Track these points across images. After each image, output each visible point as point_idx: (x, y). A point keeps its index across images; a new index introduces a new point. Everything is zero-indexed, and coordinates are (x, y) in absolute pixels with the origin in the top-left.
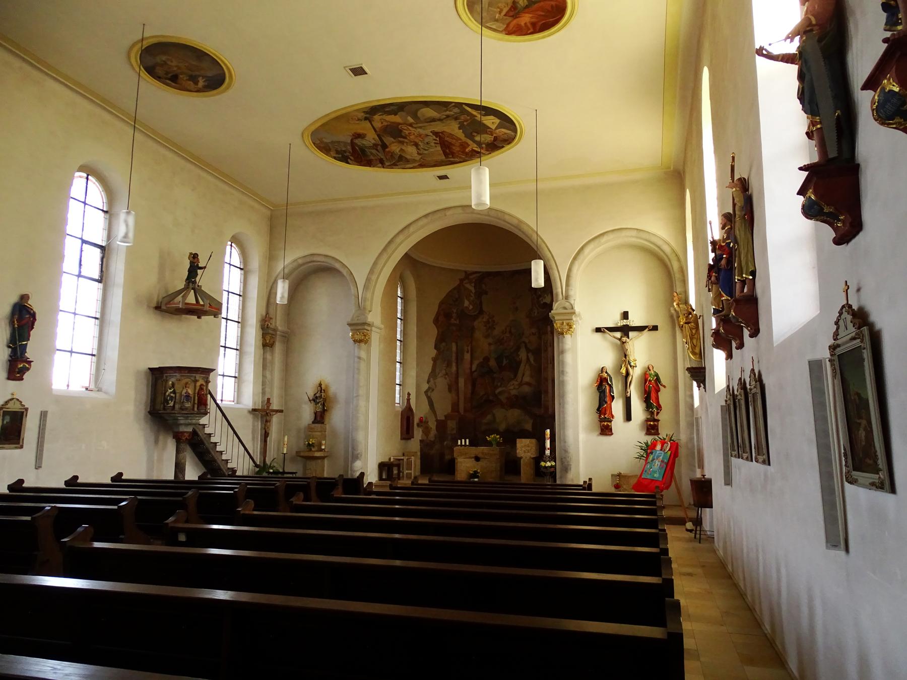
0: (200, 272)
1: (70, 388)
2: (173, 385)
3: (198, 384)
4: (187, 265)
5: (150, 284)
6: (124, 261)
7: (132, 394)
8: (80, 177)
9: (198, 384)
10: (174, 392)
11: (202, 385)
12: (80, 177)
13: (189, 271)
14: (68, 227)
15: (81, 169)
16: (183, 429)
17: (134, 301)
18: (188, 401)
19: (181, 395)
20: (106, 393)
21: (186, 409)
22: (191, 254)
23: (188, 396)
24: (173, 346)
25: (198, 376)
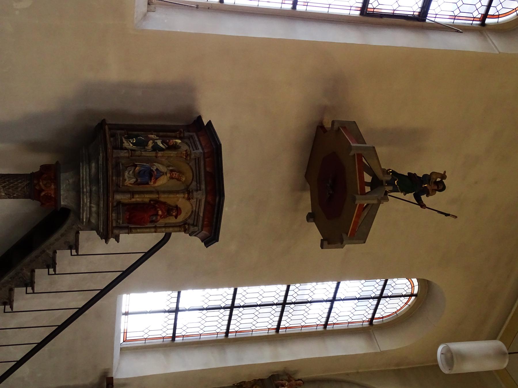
0: (410, 196)
1: (123, 317)
2: (175, 147)
3: (181, 201)
4: (421, 170)
5: (373, 112)
6: (412, 46)
7: (144, 76)
8: (413, 287)
9: (181, 201)
10: (156, 148)
11: (178, 210)
12: (413, 287)
13: (412, 176)
14: (347, 282)
15: (424, 284)
16: (66, 180)
17: (334, 75)
18: (138, 175)
19: (151, 161)
20: (145, 16)
21: (119, 174)
22: (443, 176)
23: (151, 175)
24: (257, 170)
25: (200, 196)
